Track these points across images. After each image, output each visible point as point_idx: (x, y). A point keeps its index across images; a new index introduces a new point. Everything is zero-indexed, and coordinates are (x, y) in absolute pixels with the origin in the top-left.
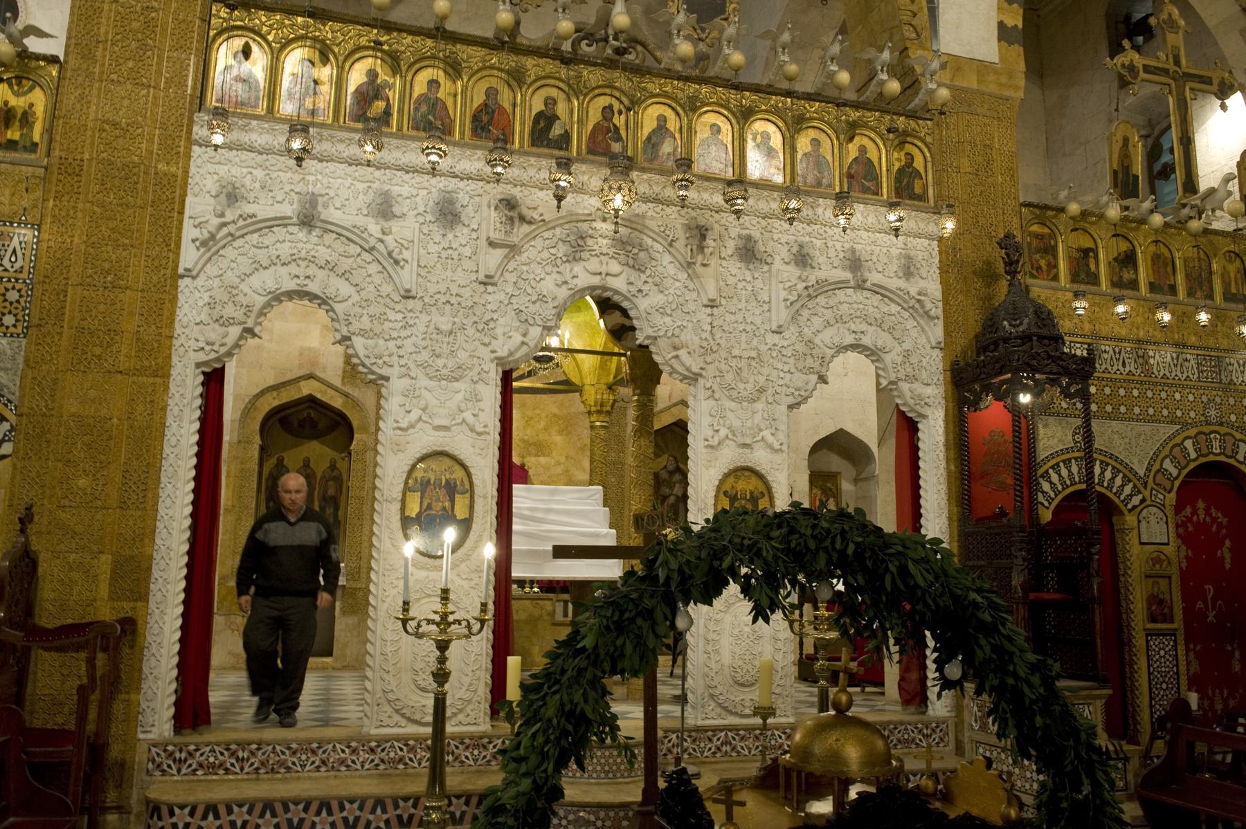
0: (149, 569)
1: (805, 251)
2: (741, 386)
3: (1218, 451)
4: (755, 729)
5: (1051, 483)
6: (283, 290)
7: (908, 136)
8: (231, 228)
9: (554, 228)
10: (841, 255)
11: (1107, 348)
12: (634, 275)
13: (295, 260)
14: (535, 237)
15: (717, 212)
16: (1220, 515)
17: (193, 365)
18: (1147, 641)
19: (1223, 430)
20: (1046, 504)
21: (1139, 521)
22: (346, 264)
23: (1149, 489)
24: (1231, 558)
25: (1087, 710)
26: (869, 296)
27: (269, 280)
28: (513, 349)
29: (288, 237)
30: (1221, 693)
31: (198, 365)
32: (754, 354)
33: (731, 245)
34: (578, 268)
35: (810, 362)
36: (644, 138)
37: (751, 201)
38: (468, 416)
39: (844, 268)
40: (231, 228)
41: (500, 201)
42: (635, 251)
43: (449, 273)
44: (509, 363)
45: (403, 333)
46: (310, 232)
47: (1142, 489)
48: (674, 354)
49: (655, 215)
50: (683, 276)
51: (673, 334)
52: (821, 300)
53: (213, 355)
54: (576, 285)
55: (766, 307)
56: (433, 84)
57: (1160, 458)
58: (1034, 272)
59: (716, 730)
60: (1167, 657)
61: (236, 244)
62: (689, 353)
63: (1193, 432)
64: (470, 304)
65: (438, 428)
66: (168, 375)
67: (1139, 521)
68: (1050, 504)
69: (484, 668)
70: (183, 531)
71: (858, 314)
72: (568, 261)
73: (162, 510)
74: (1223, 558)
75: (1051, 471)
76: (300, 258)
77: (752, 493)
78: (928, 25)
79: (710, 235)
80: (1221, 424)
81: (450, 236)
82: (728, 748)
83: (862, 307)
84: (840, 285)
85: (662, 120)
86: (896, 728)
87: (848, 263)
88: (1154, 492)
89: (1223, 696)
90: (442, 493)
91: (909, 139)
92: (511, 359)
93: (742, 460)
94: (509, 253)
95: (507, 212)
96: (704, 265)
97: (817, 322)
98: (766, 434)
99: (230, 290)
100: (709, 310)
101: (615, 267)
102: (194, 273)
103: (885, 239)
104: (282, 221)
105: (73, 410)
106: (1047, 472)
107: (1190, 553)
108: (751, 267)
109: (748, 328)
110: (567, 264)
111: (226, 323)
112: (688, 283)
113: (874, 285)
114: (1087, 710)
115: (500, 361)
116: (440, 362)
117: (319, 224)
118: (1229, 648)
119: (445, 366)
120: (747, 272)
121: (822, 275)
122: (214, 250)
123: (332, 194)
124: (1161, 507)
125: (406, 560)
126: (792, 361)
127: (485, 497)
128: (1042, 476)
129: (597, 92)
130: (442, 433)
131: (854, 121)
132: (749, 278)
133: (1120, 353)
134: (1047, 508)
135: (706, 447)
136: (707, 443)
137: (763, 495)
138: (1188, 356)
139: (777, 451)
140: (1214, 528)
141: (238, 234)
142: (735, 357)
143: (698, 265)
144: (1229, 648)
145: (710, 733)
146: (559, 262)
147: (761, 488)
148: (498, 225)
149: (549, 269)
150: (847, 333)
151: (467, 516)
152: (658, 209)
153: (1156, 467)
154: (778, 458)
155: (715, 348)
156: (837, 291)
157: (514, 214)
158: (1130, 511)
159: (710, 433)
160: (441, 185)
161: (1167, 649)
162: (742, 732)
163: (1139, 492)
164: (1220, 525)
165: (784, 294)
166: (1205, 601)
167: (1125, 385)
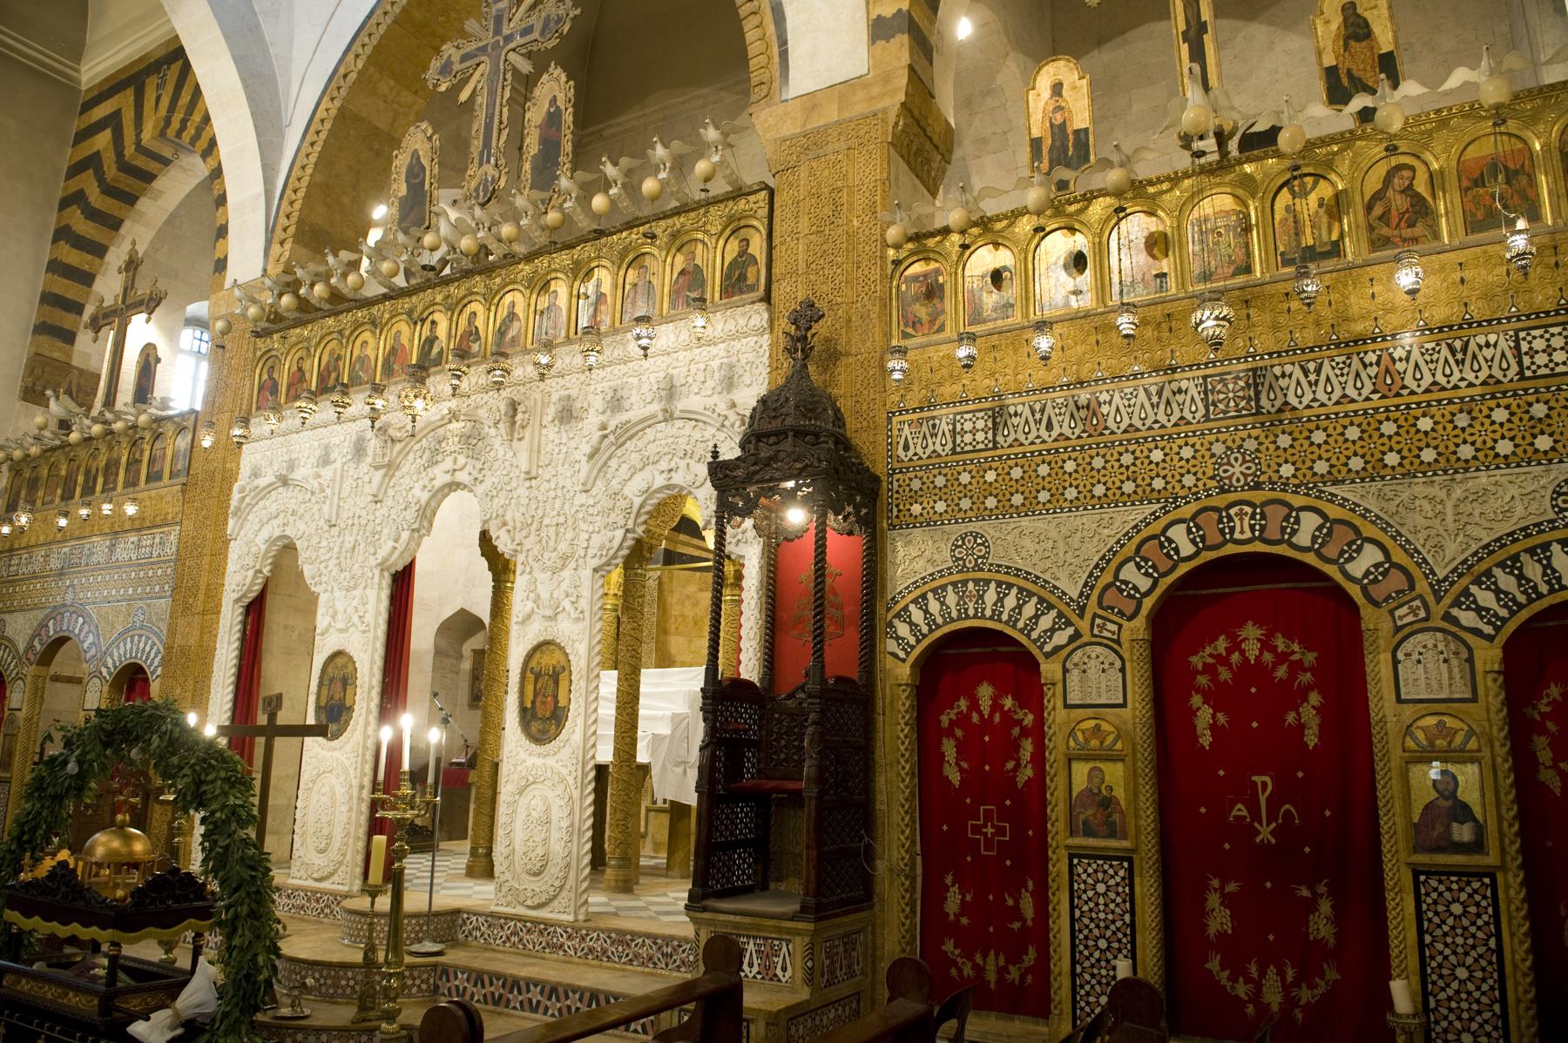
1: (619, 394)
3: (1248, 535)
4: (540, 923)
5: (911, 623)
6: (655, 487)
8: (247, 500)
10: (655, 388)
11: (1020, 409)
16: (1296, 647)
18: (1071, 866)
19: (1258, 497)
20: (902, 654)
21: (1065, 671)
23: (1088, 616)
24: (1321, 726)
25: (784, 949)
30: (1281, 973)
32: (562, 520)
33: (552, 411)
37: (607, 352)
47: (1074, 618)
57: (1389, 543)
58: (909, 330)
59: (508, 918)
60: (1112, 895)
63: (1187, 511)
65: (341, 631)
67: (1065, 671)
68: (908, 654)
71: (666, 450)
74: (1301, 727)
75: (912, 607)
77: (554, 668)
79: (521, 409)
80: (1258, 486)
82: (478, 934)
83: (670, 440)
86: (680, 946)
88: (1098, 621)
89: (1283, 979)
100: (527, 484)
103: (658, 363)
104: (270, 488)
106: (905, 609)
107: (1222, 718)
108: (568, 427)
113: (681, 411)
114: (784, 949)
118: (1305, 893)
124: (1114, 645)
128: (898, 616)
133: (1042, 411)
134: (903, 661)
138: (1184, 385)
139: (578, 619)
140: (1281, 672)
144: (1305, 893)
145: (502, 921)
147: (563, 663)
153: (1107, 578)
156: (648, 430)
158: (1047, 655)
161: (1112, 882)
162: (528, 924)
163: (1069, 623)
164: (1297, 667)
166: (1253, 808)
167: (1048, 458)
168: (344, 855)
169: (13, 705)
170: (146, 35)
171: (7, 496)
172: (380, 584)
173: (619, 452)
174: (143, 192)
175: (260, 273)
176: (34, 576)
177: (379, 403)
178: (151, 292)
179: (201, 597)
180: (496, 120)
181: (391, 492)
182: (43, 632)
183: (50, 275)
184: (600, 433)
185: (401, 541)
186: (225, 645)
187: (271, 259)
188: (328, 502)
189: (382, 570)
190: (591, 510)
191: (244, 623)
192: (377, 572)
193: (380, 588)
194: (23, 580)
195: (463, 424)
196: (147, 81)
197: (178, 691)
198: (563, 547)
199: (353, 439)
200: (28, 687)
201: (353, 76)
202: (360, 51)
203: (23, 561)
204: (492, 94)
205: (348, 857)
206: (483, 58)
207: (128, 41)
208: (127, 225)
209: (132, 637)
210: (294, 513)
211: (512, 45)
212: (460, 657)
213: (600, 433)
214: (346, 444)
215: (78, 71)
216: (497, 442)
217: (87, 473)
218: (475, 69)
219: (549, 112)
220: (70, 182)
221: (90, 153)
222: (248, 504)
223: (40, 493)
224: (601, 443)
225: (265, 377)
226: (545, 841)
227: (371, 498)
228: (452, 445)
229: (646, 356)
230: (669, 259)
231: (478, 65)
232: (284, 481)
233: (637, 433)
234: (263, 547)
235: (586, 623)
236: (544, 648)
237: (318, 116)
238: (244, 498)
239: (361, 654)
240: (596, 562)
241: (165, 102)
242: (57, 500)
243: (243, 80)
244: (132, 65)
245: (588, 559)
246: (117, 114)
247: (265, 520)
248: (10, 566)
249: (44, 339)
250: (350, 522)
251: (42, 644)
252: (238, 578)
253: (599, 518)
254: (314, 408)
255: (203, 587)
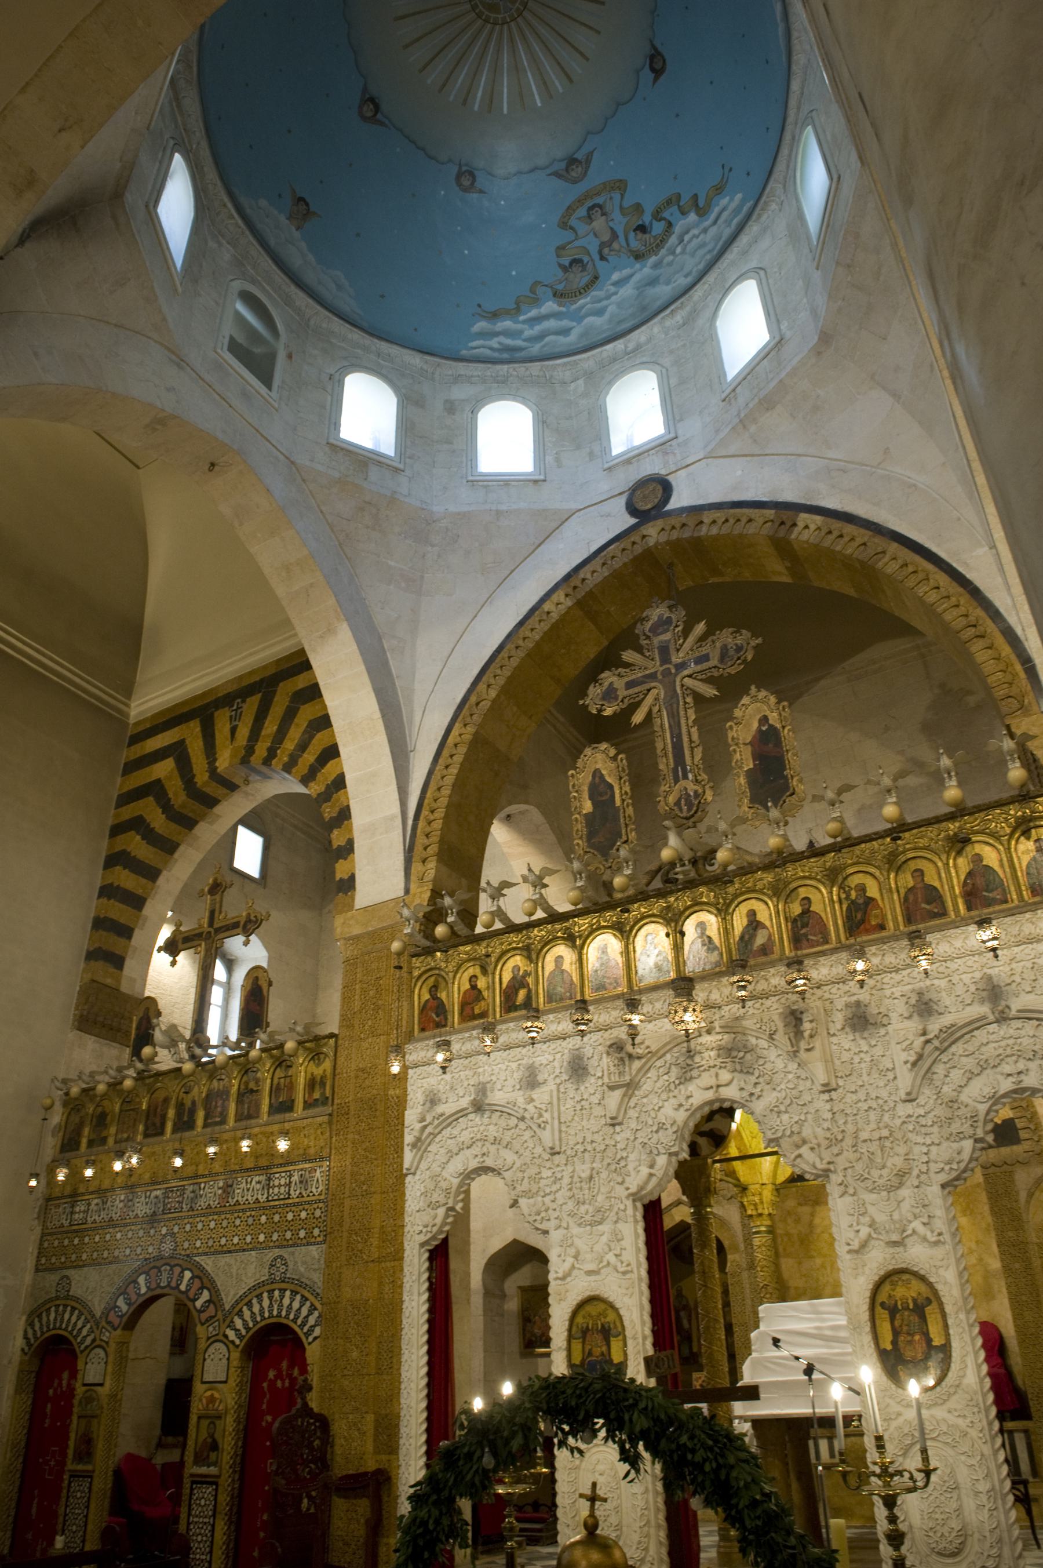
0: (397, 1426)
1: (926, 997)
2: (875, 1173)
6: (1001, 1092)
7: (1030, 820)
8: (429, 1129)
9: (664, 1055)
10: (973, 988)
12: (739, 1080)
13: (1002, 1060)
14: (649, 1069)
15: (818, 988)
17: (417, 1246)
22: (507, 1137)
26: (1020, 1026)
27: (457, 1165)
28: (641, 1183)
29: (470, 1124)
31: (422, 1245)
32: (885, 1133)
33: (839, 1018)
34: (691, 1087)
35: (956, 1127)
36: (737, 939)
38: (611, 1257)
39: (982, 1001)
40: (936, 1043)
41: (611, 1046)
42: (741, 1054)
43: (584, 1123)
44: (645, 1195)
45: (554, 1188)
46: (482, 1116)
48: (796, 1153)
49: (755, 1012)
50: (792, 1066)
51: (792, 1132)
52: (958, 1048)
53: (429, 1235)
54: (692, 1105)
55: (890, 1075)
56: (473, 978)
61: (437, 1140)
62: (812, 1149)
64: (603, 1147)
65: (589, 1273)
66: (402, 1259)
69: (653, 1523)
70: (421, 1390)
71: (1009, 1051)
72: (680, 1084)
73: (404, 1374)
76: (1007, 1056)
77: (915, 1300)
78: (1029, 688)
79: (806, 1018)
81: (582, 1088)
83: (1011, 1042)
84: (977, 1024)
85: (752, 914)
87: (985, 994)
90: (598, 1338)
91: (1032, 824)
92: (644, 1192)
93: (893, 1262)
94: (627, 1091)
95: (617, 1055)
96: (808, 1050)
97: (956, 1075)
98: (917, 1225)
99: (951, 1104)
100: (826, 1096)
101: (725, 1076)
102: (412, 1171)
103: (969, 963)
104: (462, 1113)
105: (348, 1296)
108: (866, 1034)
109: (874, 1105)
110: (681, 1087)
111: (957, 1139)
112: (800, 1072)
113: (1019, 1011)
115: (635, 1197)
116: (583, 1209)
117: (487, 1107)
119: (587, 1213)
120: (862, 1042)
121: (947, 1020)
122: (423, 1148)
123: (494, 1078)
125: (836, 1403)
126: (935, 1129)
127: (635, 1338)
129: (687, 913)
130: (593, 1278)
131: (955, 834)
132: (865, 1048)
135: (849, 1252)
136: (849, 1248)
137: (929, 1301)
139: (936, 1243)
141: (437, 1131)
142: (865, 1141)
143: (802, 1052)
146: (672, 1086)
148: (612, 1069)
149: (664, 1096)
150: (1000, 1078)
151: (943, 1342)
152: (757, 1005)
154: (939, 1252)
155: (840, 1137)
156: (976, 1033)
157: (623, 1055)
159: (852, 1235)
160: (570, 1046)
165: (904, 1056)
168: (646, 1549)
169: (90, 1379)
170: (213, 672)
171: (61, 1134)
172: (635, 1216)
173: (944, 1057)
174: (203, 817)
175: (401, 893)
176: (111, 1223)
177: (636, 1019)
178: (249, 915)
179: (375, 1242)
180: (685, 739)
181: (633, 1113)
182: (131, 1289)
183: (104, 900)
184: (923, 1039)
185: (657, 1167)
186: (415, 1297)
187: (413, 878)
188: (548, 1127)
189: (634, 1201)
190: (923, 1121)
191: (430, 1269)
192: (629, 1203)
193: (636, 1221)
194: (95, 1229)
195: (719, 1037)
196: (216, 714)
197: (355, 1354)
198: (898, 1162)
199: (566, 1057)
200: (111, 1359)
201: (485, 705)
202: (492, 681)
203: (93, 1207)
204: (674, 716)
205: (652, 1551)
206: (653, 684)
207: (189, 679)
208: (182, 848)
209: (271, 1292)
210: (496, 1141)
211: (686, 672)
212: (503, 1296)
213: (923, 1039)
214: (556, 1064)
215: (128, 706)
216: (772, 1054)
217: (180, 1106)
218: (646, 695)
219: (759, 731)
220: (120, 810)
221: (148, 780)
222: (430, 1134)
223: (113, 1130)
224: (923, 1049)
225: (426, 996)
226: (959, 1510)
227: (609, 1121)
228: (709, 1057)
229: (996, 956)
230: (951, 862)
231: (649, 690)
232: (478, 1107)
233: (962, 1036)
234: (456, 1182)
235: (948, 1247)
236: (895, 1278)
237: (451, 740)
238: (425, 1127)
239: (626, 1299)
240: (943, 1178)
241: (244, 732)
242: (139, 1138)
243: (381, 710)
244: (195, 698)
245: (932, 1174)
246: (181, 745)
247: (455, 1151)
248: (72, 1213)
249: (100, 964)
250: (580, 1148)
251: (129, 1305)
252: (425, 1218)
253: (935, 1129)
254: (540, 1025)
255: (376, 1230)
